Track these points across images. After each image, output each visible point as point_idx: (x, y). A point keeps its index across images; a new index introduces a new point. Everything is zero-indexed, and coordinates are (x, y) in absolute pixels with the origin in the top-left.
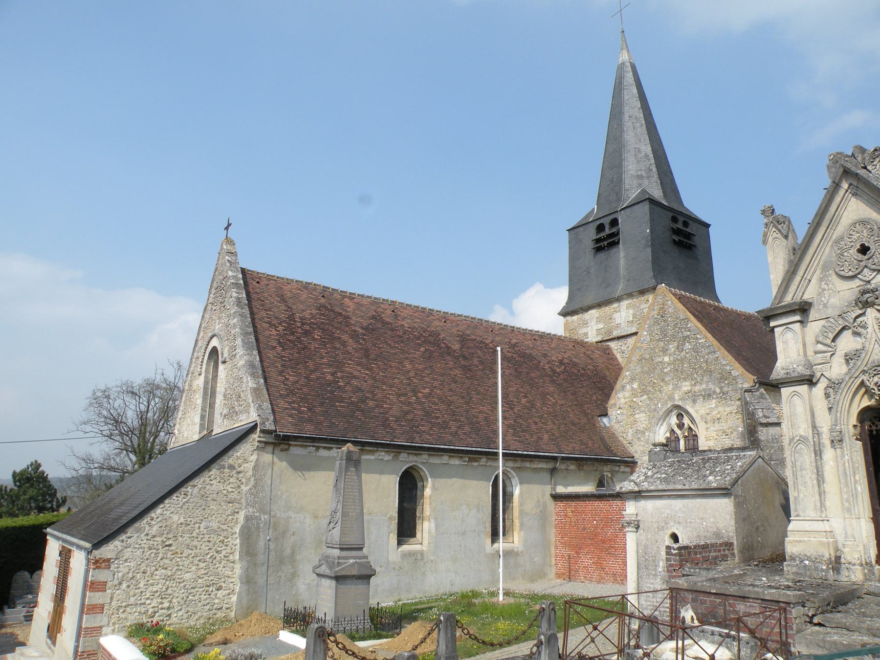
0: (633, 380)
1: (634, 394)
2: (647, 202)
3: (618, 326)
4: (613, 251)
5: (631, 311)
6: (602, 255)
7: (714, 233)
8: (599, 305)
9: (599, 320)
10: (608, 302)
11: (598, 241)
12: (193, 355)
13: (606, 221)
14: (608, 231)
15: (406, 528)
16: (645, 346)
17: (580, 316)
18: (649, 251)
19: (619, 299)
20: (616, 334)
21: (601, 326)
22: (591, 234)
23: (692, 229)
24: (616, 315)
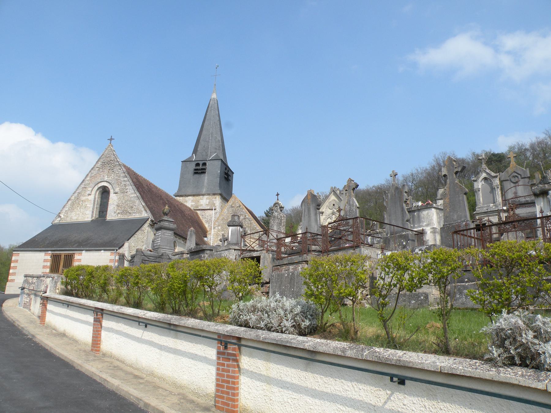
0: (219, 226)
1: (219, 230)
2: (220, 162)
3: (201, 205)
4: (202, 175)
5: (208, 201)
6: (197, 176)
7: (235, 176)
8: (194, 195)
9: (192, 201)
10: (198, 195)
11: (195, 170)
12: (77, 190)
13: (201, 163)
14: (201, 167)
15: (235, 250)
16: (225, 214)
17: (184, 198)
18: (218, 179)
19: (203, 195)
20: (200, 208)
21: (193, 204)
22: (192, 166)
23: (230, 173)
24: (201, 201)
